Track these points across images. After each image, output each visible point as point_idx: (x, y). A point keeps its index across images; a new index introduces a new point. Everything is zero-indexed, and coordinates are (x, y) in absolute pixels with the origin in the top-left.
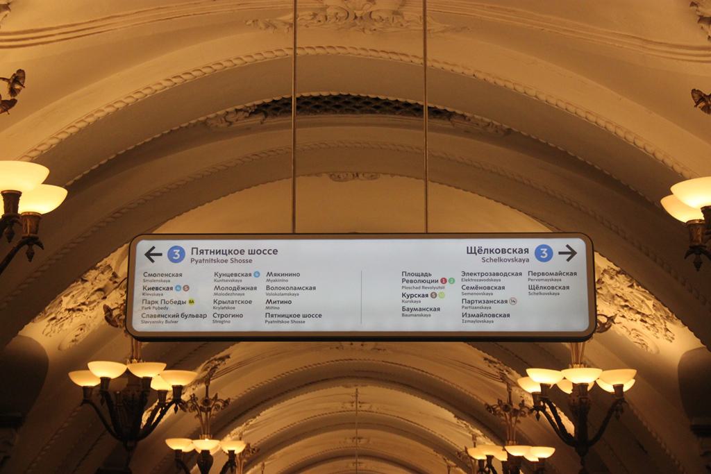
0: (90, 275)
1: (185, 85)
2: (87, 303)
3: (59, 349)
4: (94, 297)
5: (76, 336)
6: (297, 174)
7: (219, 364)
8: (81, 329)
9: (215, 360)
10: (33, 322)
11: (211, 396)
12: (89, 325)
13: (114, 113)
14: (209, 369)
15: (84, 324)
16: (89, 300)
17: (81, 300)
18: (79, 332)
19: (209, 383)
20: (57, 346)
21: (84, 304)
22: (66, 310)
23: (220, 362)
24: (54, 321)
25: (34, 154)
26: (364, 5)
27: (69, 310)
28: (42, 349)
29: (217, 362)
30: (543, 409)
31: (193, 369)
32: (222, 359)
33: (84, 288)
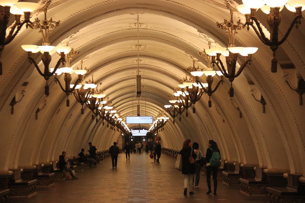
11: (48, 19)
14: (46, 3)
19: (46, 11)
30: (217, 64)
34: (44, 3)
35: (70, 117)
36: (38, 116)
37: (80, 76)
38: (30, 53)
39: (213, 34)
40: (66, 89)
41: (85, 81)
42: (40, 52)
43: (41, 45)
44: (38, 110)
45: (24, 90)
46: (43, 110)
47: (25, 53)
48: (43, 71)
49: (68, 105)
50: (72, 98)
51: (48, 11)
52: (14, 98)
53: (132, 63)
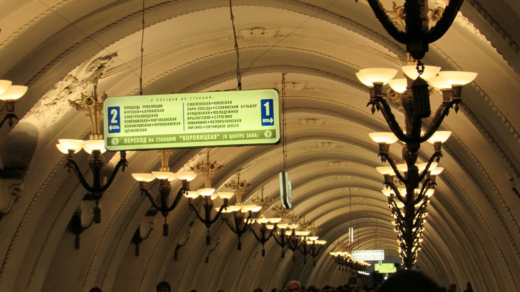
0: (59, 84)
1: (234, 159)
2: (59, 98)
3: (44, 127)
4: (63, 94)
5: (55, 118)
6: (232, 5)
7: (106, 63)
8: (58, 113)
9: (100, 58)
10: (24, 118)
12: (64, 109)
13: (159, 80)
14: (94, 70)
15: (60, 109)
16: (59, 96)
17: (54, 98)
18: (57, 115)
19: (97, 83)
20: (43, 126)
21: (57, 99)
22: (45, 105)
23: (106, 61)
24: (38, 113)
25: (82, 137)
26: (255, 199)
27: (47, 105)
28: (36, 128)
29: (103, 62)
31: (400, 269)
32: (109, 57)
33: (55, 92)
34: (91, 71)
35: (255, 256)
36: (81, 241)
37: (226, 200)
38: (141, 183)
39: (461, 162)
40: (237, 229)
41: (69, 100)
42: (156, 179)
43: (158, 170)
44: (179, 247)
45: (152, 221)
46: (185, 246)
47: (137, 183)
48: (303, 251)
49: (263, 254)
50: (249, 240)
51: (100, 81)
52: (138, 232)
53: (316, 147)
